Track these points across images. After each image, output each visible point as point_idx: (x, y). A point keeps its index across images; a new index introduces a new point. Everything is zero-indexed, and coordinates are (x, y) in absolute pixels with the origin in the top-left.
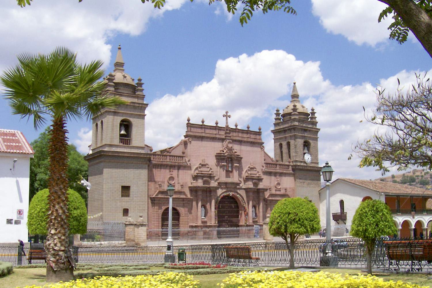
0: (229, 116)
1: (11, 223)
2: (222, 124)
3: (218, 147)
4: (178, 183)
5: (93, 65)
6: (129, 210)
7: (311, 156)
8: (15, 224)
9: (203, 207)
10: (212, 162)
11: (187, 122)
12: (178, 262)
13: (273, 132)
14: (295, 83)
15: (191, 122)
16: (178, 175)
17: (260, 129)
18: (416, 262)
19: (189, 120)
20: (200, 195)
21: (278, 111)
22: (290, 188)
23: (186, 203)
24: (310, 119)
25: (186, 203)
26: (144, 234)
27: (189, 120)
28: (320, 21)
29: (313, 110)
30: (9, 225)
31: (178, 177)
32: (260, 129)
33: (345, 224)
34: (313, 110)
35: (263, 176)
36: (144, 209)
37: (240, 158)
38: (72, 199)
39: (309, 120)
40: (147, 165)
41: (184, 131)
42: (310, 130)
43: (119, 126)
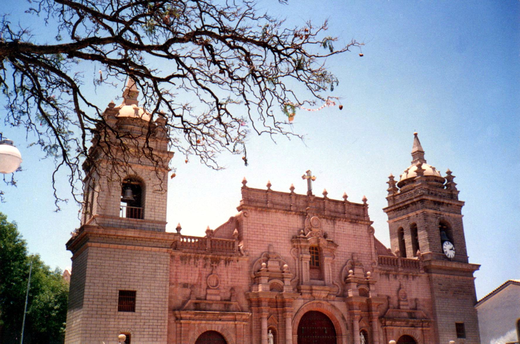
2: (301, 190)
6: (132, 336)
13: (387, 210)
15: (249, 185)
19: (244, 182)
22: (424, 300)
27: (244, 182)
29: (449, 173)
32: (365, 200)
34: (449, 173)
41: (238, 199)
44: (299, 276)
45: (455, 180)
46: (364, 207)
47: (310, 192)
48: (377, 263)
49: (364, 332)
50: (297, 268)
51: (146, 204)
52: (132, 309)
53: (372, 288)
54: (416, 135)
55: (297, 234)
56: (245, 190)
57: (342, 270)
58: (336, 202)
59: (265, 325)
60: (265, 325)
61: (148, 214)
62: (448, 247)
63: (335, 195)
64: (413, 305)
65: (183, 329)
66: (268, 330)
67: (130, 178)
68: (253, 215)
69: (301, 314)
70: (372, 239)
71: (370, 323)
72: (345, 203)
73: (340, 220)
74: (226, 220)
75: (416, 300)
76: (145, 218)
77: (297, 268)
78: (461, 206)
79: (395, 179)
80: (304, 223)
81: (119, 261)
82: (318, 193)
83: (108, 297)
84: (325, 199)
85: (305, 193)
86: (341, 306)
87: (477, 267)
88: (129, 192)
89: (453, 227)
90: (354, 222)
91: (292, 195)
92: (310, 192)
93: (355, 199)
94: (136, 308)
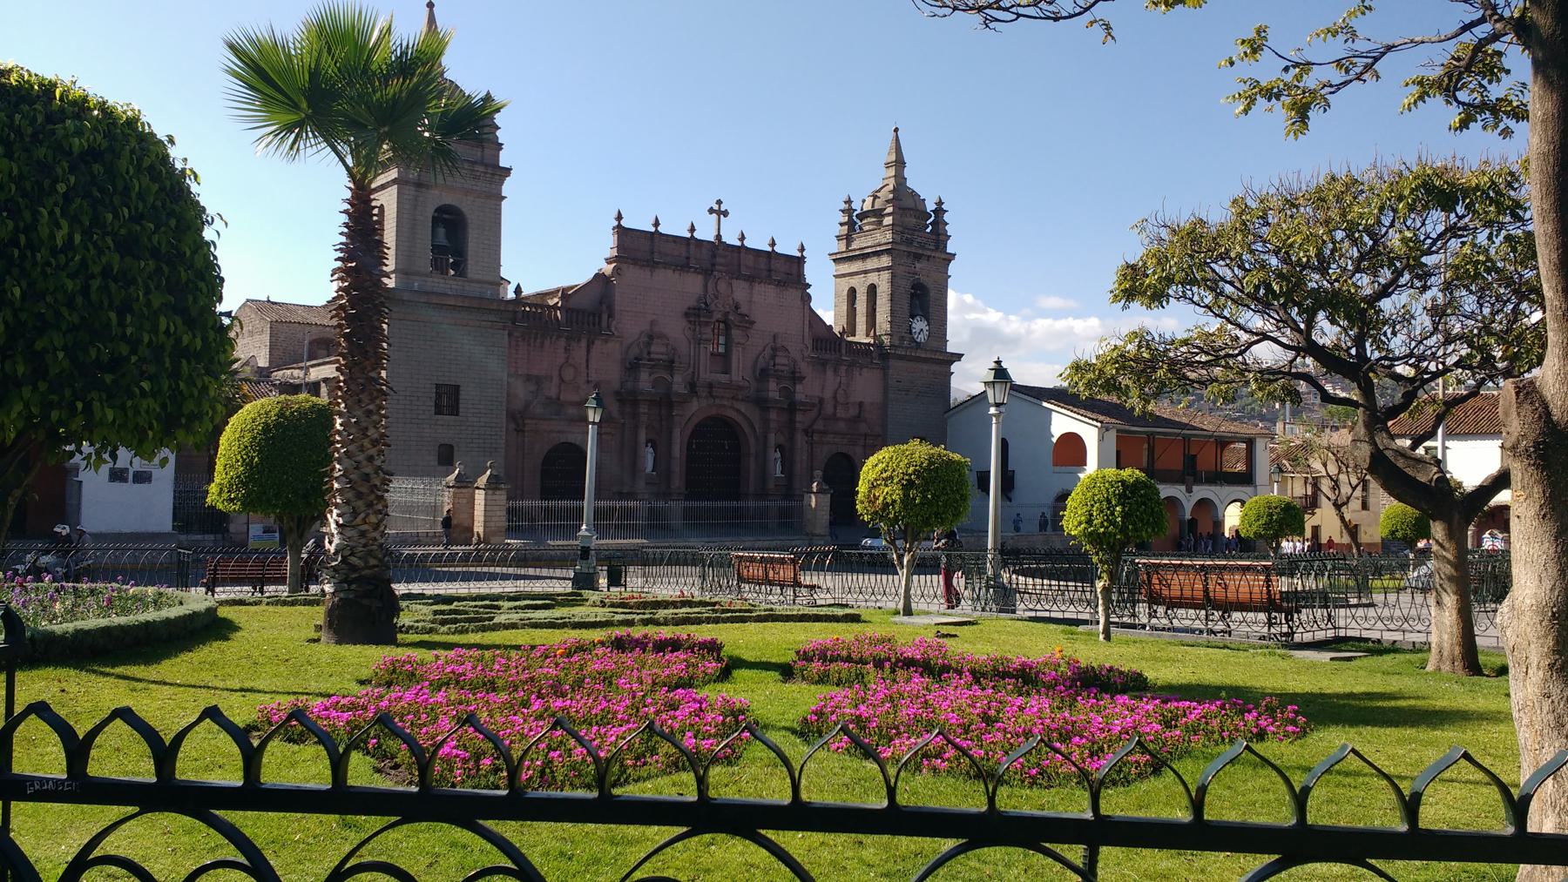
0: (726, 214)
1: (125, 480)
2: (706, 233)
3: (691, 286)
4: (588, 382)
5: (1393, 703)
6: (456, 448)
7: (929, 325)
8: (134, 482)
9: (650, 445)
10: (676, 330)
11: (616, 223)
12: (606, 590)
13: (834, 257)
14: (896, 130)
15: (625, 223)
16: (587, 361)
17: (802, 249)
18: (1217, 614)
19: (619, 217)
20: (644, 413)
21: (849, 202)
22: (872, 404)
23: (605, 433)
24: (930, 228)
25: (605, 433)
26: (498, 513)
27: (619, 217)
28: (1550, 642)
29: (940, 203)
30: (117, 484)
31: (587, 366)
32: (802, 249)
33: (1010, 500)
34: (940, 203)
35: (805, 369)
36: (494, 446)
37: (747, 322)
38: (1079, 705)
39: (928, 230)
40: (507, 332)
41: (607, 245)
42: (929, 257)
43: (430, 224)
44: (694, 368)
45: (946, 217)
46: (800, 261)
47: (719, 237)
48: (810, 348)
49: (780, 447)
50: (692, 354)
51: (470, 253)
52: (454, 411)
53: (799, 387)
54: (896, 130)
55: (695, 304)
56: (621, 231)
57: (758, 357)
58: (758, 253)
59: (642, 436)
60: (642, 436)
61: (474, 268)
62: (919, 325)
63: (758, 242)
64: (853, 412)
65: (526, 439)
66: (647, 442)
67: (442, 210)
68: (633, 273)
69: (695, 420)
70: (807, 311)
71: (791, 439)
72: (771, 255)
73: (760, 283)
74: (590, 276)
75: (861, 404)
76: (469, 276)
77: (692, 354)
78: (950, 261)
79: (854, 206)
80: (706, 286)
81: (559, 432)
82: (731, 238)
83: (419, 394)
84: (741, 250)
85: (712, 239)
86: (752, 413)
87: (959, 357)
88: (441, 231)
89: (932, 294)
90: (781, 284)
91: (691, 243)
92: (719, 237)
93: (787, 248)
94: (461, 410)
